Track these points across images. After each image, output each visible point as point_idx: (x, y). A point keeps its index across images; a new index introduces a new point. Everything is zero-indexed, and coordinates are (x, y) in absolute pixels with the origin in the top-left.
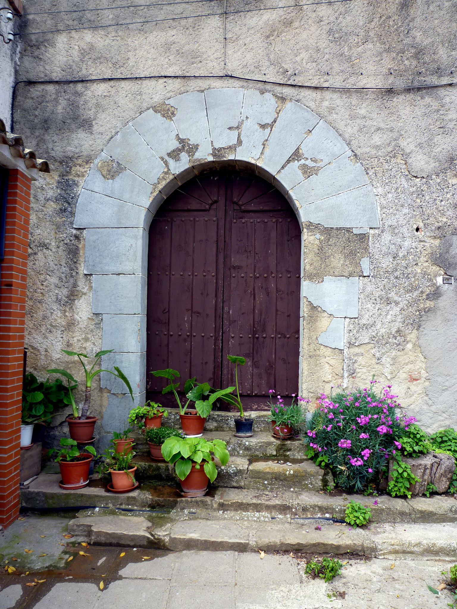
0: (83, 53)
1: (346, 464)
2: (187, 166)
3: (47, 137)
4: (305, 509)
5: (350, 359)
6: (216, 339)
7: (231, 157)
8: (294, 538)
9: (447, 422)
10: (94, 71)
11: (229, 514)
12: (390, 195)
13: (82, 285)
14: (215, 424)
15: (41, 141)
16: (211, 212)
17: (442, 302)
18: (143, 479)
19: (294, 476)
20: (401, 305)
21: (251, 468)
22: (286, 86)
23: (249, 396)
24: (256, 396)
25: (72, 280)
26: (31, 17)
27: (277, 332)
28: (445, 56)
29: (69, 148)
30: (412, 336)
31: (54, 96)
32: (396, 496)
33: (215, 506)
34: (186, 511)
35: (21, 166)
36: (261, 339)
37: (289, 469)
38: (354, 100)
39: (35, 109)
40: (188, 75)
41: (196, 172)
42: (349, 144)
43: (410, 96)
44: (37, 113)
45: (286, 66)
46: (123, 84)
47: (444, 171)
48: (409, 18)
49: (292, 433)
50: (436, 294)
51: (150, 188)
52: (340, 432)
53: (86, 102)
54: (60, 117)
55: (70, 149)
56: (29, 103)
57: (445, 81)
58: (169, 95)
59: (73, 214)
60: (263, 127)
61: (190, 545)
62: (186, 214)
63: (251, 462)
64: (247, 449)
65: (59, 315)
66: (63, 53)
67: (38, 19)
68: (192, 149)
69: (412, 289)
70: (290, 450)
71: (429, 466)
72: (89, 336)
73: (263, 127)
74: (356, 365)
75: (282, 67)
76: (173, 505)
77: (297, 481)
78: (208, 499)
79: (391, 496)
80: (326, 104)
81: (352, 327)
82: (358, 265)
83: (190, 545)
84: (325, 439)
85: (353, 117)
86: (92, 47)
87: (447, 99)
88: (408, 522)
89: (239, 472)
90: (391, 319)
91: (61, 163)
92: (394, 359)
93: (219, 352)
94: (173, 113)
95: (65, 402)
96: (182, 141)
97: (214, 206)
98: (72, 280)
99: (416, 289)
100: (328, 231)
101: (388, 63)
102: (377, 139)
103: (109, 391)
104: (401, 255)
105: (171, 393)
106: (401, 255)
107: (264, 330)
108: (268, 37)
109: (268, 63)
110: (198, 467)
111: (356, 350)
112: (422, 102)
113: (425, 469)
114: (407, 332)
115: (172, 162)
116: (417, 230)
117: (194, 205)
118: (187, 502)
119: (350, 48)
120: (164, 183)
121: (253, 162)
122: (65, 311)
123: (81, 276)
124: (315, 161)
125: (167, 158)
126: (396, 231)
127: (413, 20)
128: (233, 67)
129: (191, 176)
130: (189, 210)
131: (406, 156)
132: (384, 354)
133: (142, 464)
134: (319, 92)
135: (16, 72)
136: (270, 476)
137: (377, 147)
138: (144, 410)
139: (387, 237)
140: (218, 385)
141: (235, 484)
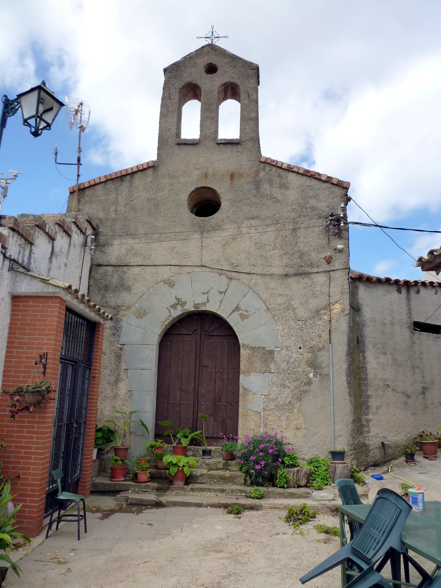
0: (128, 251)
1: (254, 469)
2: (180, 313)
3: (107, 295)
4: (232, 491)
5: (264, 417)
6: (194, 406)
7: (203, 309)
8: (223, 501)
9: (316, 453)
10: (133, 261)
11: (194, 493)
12: (286, 330)
13: (123, 375)
14: (192, 453)
15: (104, 297)
16: (193, 335)
17: (313, 387)
18: (152, 478)
19: (230, 477)
20: (291, 389)
21: (208, 473)
22: (232, 273)
23: (212, 438)
24: (215, 438)
25: (117, 372)
26: (100, 230)
27: (227, 402)
28: (315, 257)
29: (118, 301)
30: (297, 405)
31: (111, 273)
32: (280, 487)
33: (189, 490)
34: (174, 492)
35: (102, 321)
36: (219, 406)
37: (227, 474)
38: (268, 279)
39: (101, 279)
40: (182, 264)
41: (185, 315)
42: (264, 303)
43: (296, 278)
44: (102, 281)
45: (233, 261)
46: (148, 268)
47: (314, 317)
48: (297, 237)
49: (231, 457)
50: (309, 383)
51: (161, 324)
52: (251, 453)
53: (128, 277)
54: (114, 284)
55: (119, 302)
56: (98, 276)
57: (315, 270)
58: (172, 275)
59: (119, 336)
60: (220, 293)
61: (175, 504)
62: (179, 336)
63: (209, 471)
64: (208, 465)
65: (110, 391)
66: (116, 251)
67: (104, 231)
68: (183, 304)
69: (297, 380)
70: (230, 466)
71: (295, 471)
72: (125, 403)
73: (220, 293)
74: (267, 421)
75: (231, 262)
76: (168, 489)
77: (231, 480)
78: (185, 486)
79: (277, 487)
80: (253, 281)
81: (265, 400)
82: (268, 366)
83: (175, 504)
84: (245, 457)
85: (267, 289)
86: (132, 248)
87: (316, 280)
88: (283, 498)
89: (202, 475)
90: (286, 395)
91: (114, 309)
92: (287, 417)
93: (196, 413)
94: (174, 285)
95: (112, 439)
96: (178, 299)
97: (195, 333)
98: (117, 372)
99: (299, 380)
100: (253, 349)
101: (285, 260)
102: (279, 300)
103: (135, 434)
104: (291, 361)
105: (169, 436)
106: (291, 361)
107: (220, 401)
108: (224, 246)
109: (223, 260)
110: (181, 469)
111: (268, 412)
112: (302, 281)
113: (294, 473)
114: (294, 403)
115: (172, 311)
116: (300, 348)
117: (184, 331)
118: (175, 487)
119: (266, 252)
120: (168, 321)
121: (215, 311)
122: (113, 389)
123: (122, 370)
124: (247, 312)
125: (170, 308)
126: (289, 349)
127: (299, 238)
128: (206, 261)
129: (183, 316)
130: (181, 334)
131: (294, 309)
132: (282, 415)
133: (153, 471)
134: (250, 275)
135: (92, 259)
136: (217, 477)
137: (280, 305)
138: (154, 443)
139: (284, 352)
140: (194, 429)
141: (200, 481)
